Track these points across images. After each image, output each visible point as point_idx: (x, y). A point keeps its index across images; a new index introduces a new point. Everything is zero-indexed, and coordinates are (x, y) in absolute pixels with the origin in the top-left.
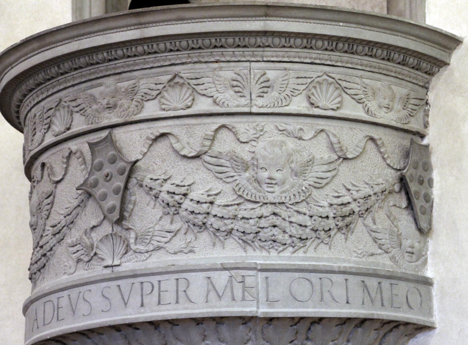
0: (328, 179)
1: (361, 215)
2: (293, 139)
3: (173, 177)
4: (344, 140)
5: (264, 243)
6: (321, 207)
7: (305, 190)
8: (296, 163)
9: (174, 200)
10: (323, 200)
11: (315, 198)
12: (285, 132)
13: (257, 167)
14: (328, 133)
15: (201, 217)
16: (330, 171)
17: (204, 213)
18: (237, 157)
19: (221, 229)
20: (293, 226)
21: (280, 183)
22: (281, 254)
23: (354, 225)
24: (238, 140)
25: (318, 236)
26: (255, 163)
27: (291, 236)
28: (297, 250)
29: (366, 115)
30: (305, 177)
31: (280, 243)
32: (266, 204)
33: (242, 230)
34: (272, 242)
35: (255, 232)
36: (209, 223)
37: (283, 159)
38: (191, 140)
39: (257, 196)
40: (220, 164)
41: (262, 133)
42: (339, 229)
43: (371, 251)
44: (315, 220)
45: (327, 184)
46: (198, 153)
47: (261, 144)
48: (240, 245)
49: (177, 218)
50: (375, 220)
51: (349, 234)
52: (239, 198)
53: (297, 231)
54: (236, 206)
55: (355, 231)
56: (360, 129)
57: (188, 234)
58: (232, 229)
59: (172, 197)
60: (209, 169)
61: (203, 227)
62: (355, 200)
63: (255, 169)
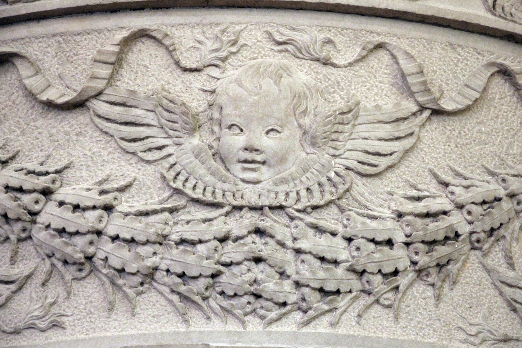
0: (394, 156)
1: (476, 244)
2: (308, 63)
3: (21, 154)
4: (435, 72)
5: (234, 302)
6: (375, 218)
7: (336, 179)
8: (315, 115)
9: (19, 205)
10: (380, 204)
11: (360, 198)
12: (289, 47)
13: (220, 125)
14: (394, 52)
15: (79, 241)
16: (398, 139)
17: (88, 232)
18: (171, 101)
19: (127, 270)
20: (303, 261)
21: (272, 161)
22: (274, 328)
23: (458, 265)
24: (177, 63)
25: (367, 287)
26: (216, 115)
27: (298, 284)
28: (314, 318)
29: (489, 16)
30: (335, 148)
31: (271, 300)
32: (240, 208)
33: (179, 271)
34: (252, 299)
35: (209, 273)
36: (101, 255)
37: (283, 105)
38: (69, 70)
39: (217, 190)
40: (133, 120)
41: (234, 49)
42: (421, 273)
43: (501, 331)
44: (358, 249)
45: (390, 167)
46: (80, 94)
47: (231, 73)
48: (174, 306)
49: (26, 248)
50: (511, 258)
51: (446, 286)
52: (174, 197)
53: (313, 272)
54: (166, 214)
55: (462, 280)
56: (475, 49)
57: (50, 285)
58: (156, 269)
59: (16, 199)
60: (106, 133)
61: (87, 267)
62: (460, 207)
63: (216, 129)
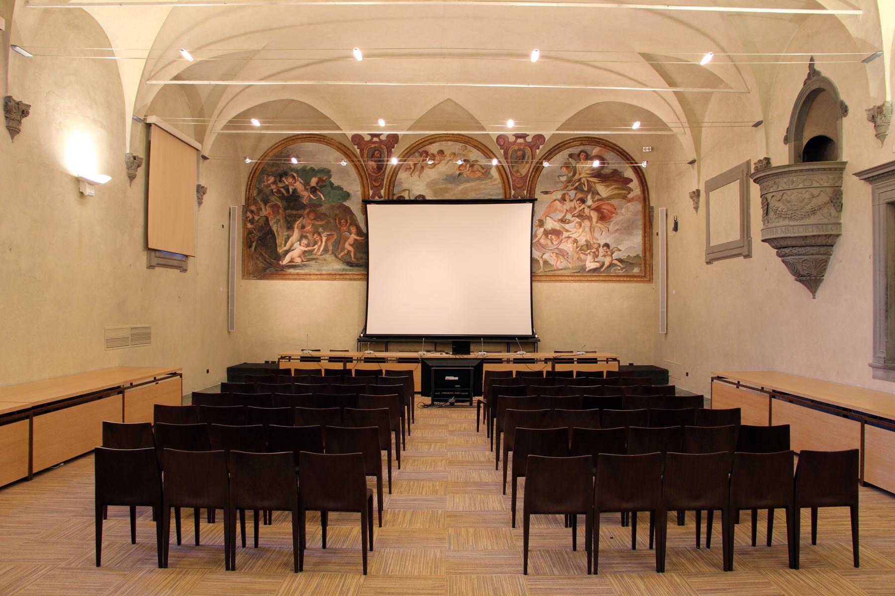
10: (808, 208)
